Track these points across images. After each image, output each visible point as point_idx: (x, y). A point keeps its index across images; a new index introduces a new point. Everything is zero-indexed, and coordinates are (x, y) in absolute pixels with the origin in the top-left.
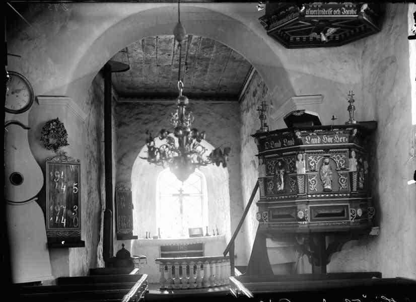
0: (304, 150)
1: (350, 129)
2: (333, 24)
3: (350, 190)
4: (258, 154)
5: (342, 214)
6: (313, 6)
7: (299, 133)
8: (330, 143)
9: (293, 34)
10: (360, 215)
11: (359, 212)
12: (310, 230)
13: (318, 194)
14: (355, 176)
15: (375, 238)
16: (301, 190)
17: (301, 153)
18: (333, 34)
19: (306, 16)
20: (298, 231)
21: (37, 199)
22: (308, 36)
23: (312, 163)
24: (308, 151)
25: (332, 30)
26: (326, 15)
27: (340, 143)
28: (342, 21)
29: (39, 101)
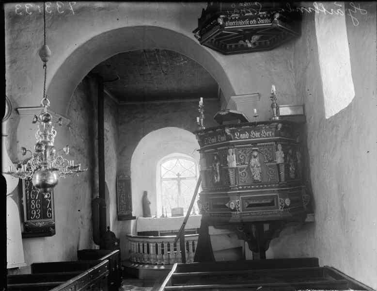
0: (233, 145)
1: (276, 124)
2: (258, 32)
3: (278, 181)
4: (199, 148)
5: (272, 204)
6: (231, 19)
7: (228, 130)
8: (258, 138)
9: (229, 42)
10: (288, 205)
11: (287, 202)
12: (242, 220)
13: (249, 186)
14: (282, 168)
15: (312, 224)
16: (232, 181)
17: (232, 148)
18: (258, 41)
19: (226, 28)
20: (231, 221)
21: (12, 195)
22: (236, 44)
23: (242, 157)
24: (237, 146)
25: (255, 38)
26: (244, 25)
27: (266, 137)
28: (264, 29)
29: (19, 112)
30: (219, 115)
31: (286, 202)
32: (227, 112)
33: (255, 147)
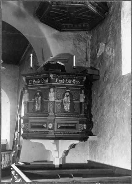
8: (70, 84)
30: (73, 56)
31: (84, 127)
32: (56, 63)
33: (68, 89)
